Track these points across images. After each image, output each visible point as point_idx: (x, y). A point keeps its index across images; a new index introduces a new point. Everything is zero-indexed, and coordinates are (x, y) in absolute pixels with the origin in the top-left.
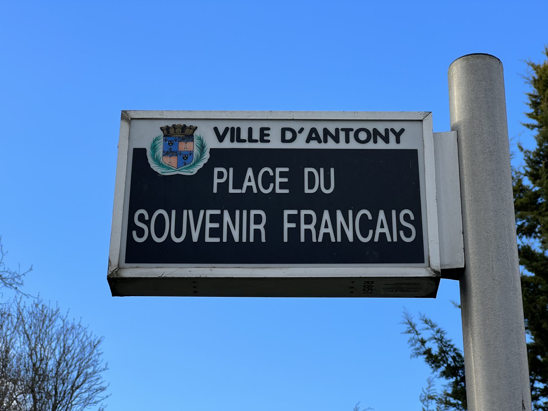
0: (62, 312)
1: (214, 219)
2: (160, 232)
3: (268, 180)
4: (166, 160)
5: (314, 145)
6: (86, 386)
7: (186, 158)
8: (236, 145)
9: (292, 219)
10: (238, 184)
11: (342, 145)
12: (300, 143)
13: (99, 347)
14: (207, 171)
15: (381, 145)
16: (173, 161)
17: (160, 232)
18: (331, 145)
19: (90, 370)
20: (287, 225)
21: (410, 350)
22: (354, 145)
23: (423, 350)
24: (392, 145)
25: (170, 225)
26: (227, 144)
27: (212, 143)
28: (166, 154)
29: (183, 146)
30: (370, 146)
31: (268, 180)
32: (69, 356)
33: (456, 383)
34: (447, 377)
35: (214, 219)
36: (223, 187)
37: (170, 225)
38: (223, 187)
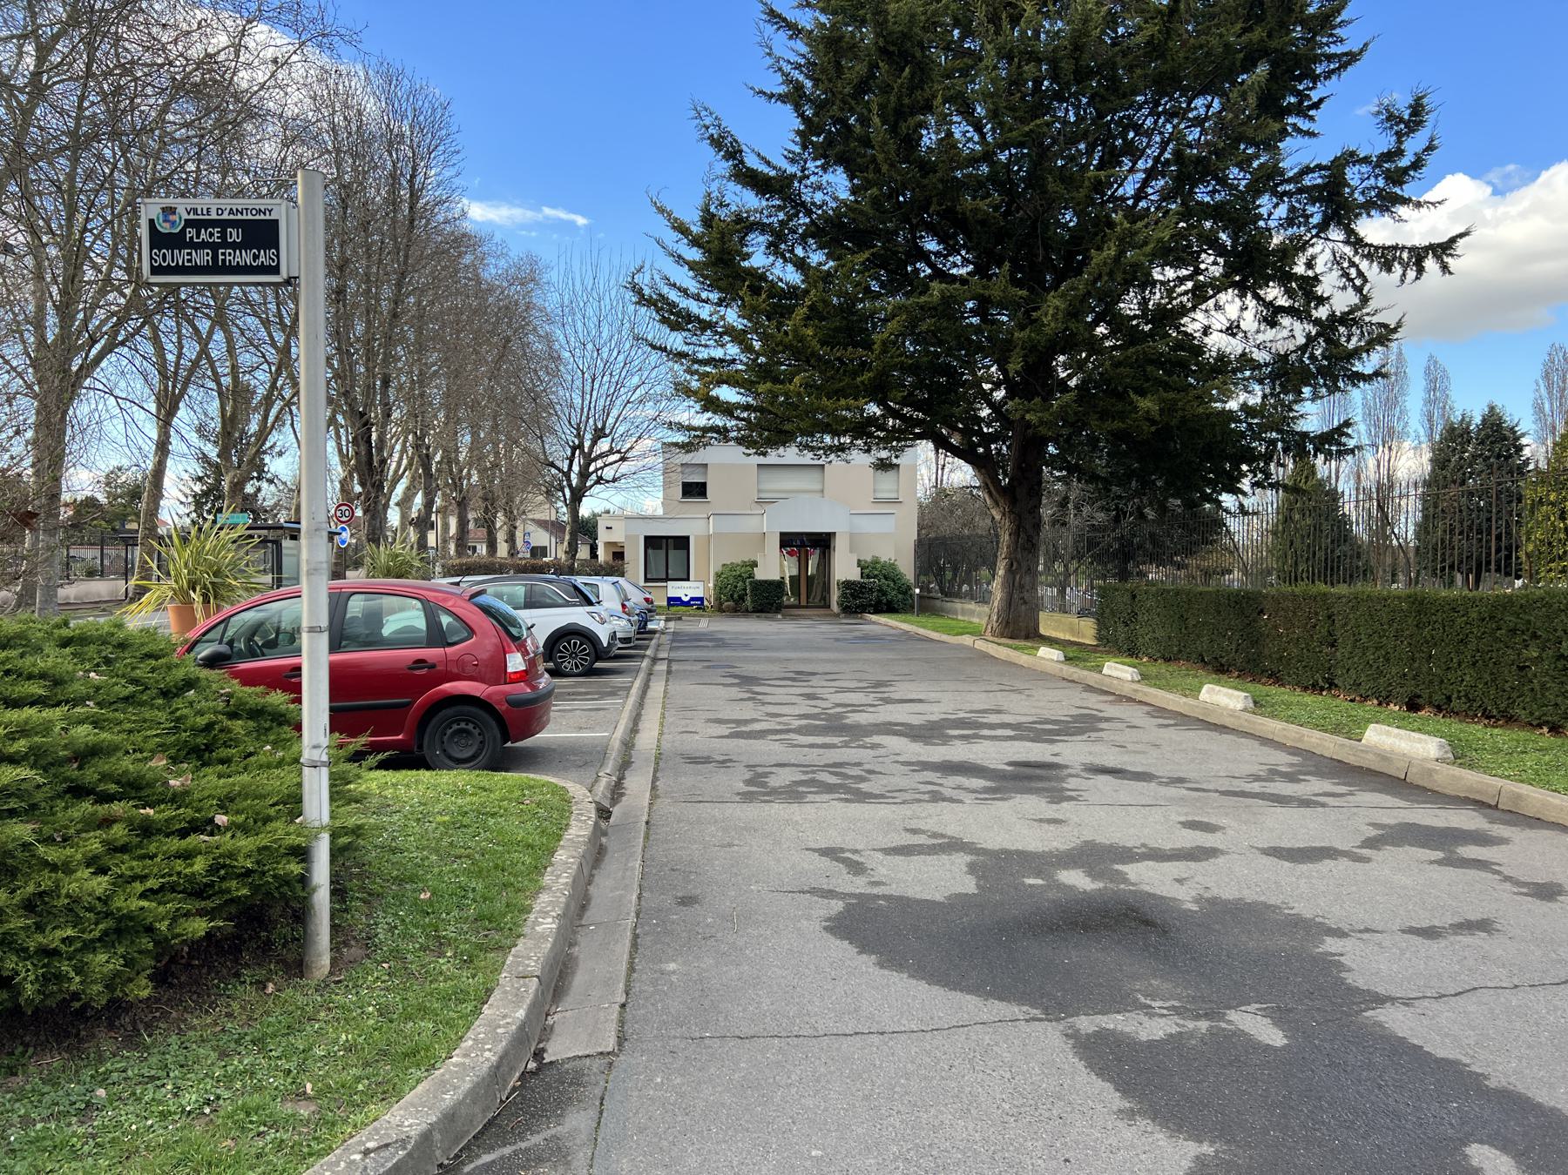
0: (408, 72)
1: (188, 254)
2: (164, 261)
3: (211, 235)
4: (164, 225)
5: (232, 217)
6: (441, 148)
7: (173, 223)
8: (196, 217)
9: (223, 254)
10: (198, 237)
11: (245, 217)
12: (225, 216)
13: (450, 108)
14: (183, 230)
15: (262, 217)
16: (167, 225)
17: (164, 261)
18: (239, 217)
19: (444, 132)
20: (221, 257)
21: (697, 135)
22: (250, 217)
23: (707, 135)
24: (267, 217)
25: (169, 258)
26: (192, 216)
27: (185, 216)
28: (165, 221)
29: (172, 218)
30: (257, 217)
31: (211, 235)
32: (421, 118)
33: (735, 166)
34: (727, 160)
35: (188, 254)
36: (191, 238)
37: (169, 258)
38: (191, 238)
